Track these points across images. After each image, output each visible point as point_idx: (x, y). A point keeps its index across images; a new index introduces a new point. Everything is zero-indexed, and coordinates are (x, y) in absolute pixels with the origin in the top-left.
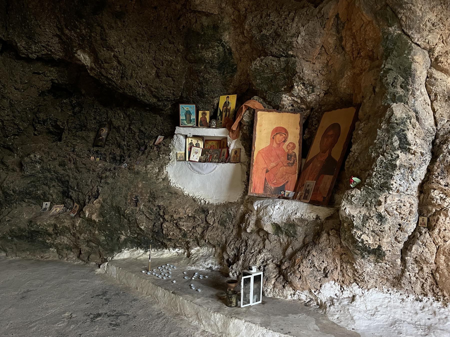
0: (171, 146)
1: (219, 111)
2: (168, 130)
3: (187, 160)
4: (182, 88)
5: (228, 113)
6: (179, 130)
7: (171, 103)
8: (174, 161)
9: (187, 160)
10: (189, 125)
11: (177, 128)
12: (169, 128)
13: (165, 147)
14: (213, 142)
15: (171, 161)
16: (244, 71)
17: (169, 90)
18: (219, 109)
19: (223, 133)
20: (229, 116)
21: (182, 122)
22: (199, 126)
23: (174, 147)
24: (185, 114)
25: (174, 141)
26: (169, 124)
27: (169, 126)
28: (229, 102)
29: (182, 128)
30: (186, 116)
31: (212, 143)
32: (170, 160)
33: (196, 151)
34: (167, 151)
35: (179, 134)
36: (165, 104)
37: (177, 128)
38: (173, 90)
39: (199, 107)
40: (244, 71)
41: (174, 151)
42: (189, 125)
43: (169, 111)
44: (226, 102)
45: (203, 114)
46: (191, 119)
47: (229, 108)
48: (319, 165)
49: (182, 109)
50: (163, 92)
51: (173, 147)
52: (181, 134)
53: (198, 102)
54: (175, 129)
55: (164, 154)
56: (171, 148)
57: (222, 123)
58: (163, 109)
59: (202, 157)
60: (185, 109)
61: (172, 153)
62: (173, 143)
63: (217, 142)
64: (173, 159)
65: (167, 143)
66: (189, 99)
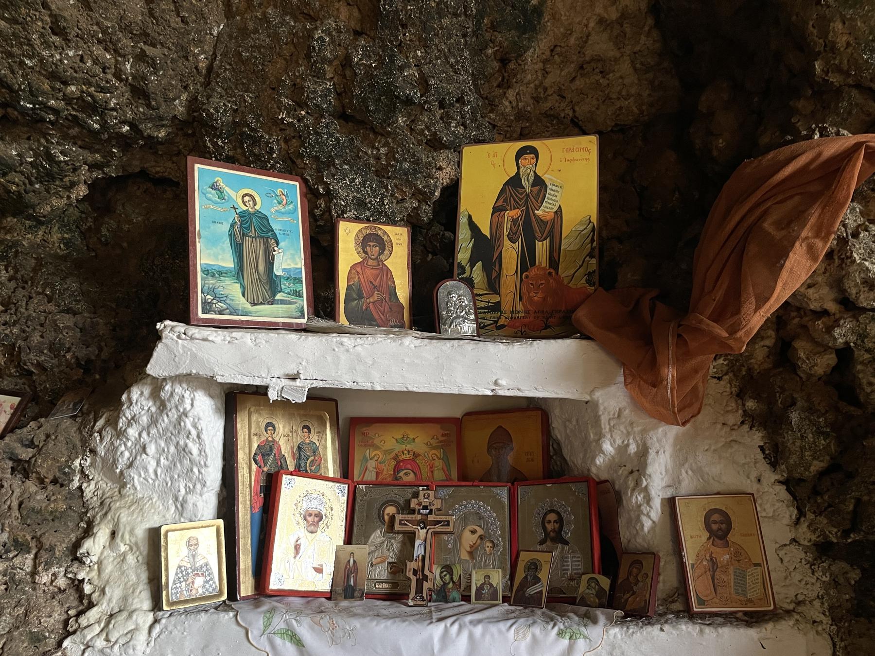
0: (84, 476)
1: (463, 234)
2: (54, 349)
3: (246, 586)
4: (203, 65)
5: (542, 248)
6: (193, 346)
7: (93, 167)
8: (124, 609)
9: (246, 586)
10: (265, 313)
11: (170, 329)
12: (69, 337)
13: (32, 486)
14: (411, 432)
15: (93, 614)
16: (572, 40)
17: (108, 44)
18: (463, 221)
19: (566, 372)
20: (554, 262)
21: (212, 291)
22: (343, 320)
23: (121, 481)
24: (232, 235)
25: (120, 434)
26: (69, 311)
27: (66, 321)
28: (539, 182)
29: (217, 336)
30: (238, 250)
31: (404, 439)
32: (86, 604)
33: (314, 505)
34: (55, 516)
35: (179, 379)
36: (50, 158)
37: (170, 329)
38: (141, 57)
39: (329, 195)
40: (572, 40)
41: (124, 517)
42: (265, 313)
43: (56, 237)
44: (514, 182)
45: (365, 242)
46: (278, 271)
47: (545, 211)
48: (36, 411)
49: (213, 195)
50: (61, 49)
51: (107, 486)
52: (192, 380)
53: (330, 164)
54: (157, 337)
55: (21, 547)
56: (89, 490)
57: (506, 306)
58: (31, 198)
59: (360, 551)
60: (235, 196)
61: (102, 534)
62: (113, 450)
63: (436, 429)
64: (114, 594)
65: (57, 448)
66: (256, 141)
